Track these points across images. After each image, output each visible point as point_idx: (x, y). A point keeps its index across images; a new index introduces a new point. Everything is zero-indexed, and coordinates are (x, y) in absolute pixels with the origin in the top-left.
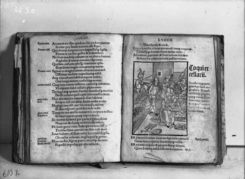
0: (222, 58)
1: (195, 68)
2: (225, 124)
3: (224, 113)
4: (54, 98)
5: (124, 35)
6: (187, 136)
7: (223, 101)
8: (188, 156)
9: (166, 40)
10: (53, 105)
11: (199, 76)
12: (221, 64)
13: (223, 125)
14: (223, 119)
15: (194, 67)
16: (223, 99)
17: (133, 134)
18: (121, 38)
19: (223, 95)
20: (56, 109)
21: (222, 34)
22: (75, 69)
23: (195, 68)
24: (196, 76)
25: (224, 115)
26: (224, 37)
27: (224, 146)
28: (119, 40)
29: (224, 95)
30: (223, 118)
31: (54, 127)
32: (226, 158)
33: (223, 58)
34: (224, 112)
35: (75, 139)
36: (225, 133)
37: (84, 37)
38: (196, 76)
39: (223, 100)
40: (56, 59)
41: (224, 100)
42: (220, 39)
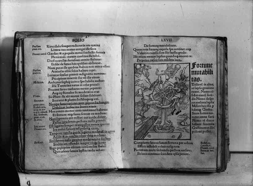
0: (225, 62)
1: (198, 65)
2: (228, 130)
3: (228, 118)
4: (51, 103)
5: (123, 37)
6: (190, 139)
7: (227, 106)
8: (200, 90)
9: (166, 40)
10: (49, 103)
11: (204, 74)
12: (225, 68)
13: (227, 130)
14: (226, 124)
15: (197, 65)
16: (227, 108)
17: (134, 139)
18: (120, 39)
19: (226, 100)
20: (53, 115)
21: (225, 36)
22: (82, 50)
23: (198, 65)
24: (202, 73)
25: (228, 121)
26: (227, 39)
27: (228, 151)
28: (118, 41)
29: (228, 100)
30: (227, 123)
31: (51, 111)
32: (229, 165)
33: (226, 61)
34: (227, 117)
35: (75, 94)
36: (229, 139)
37: (81, 39)
38: (202, 73)
39: (227, 105)
40: (52, 92)
41: (228, 105)
42: (224, 40)
